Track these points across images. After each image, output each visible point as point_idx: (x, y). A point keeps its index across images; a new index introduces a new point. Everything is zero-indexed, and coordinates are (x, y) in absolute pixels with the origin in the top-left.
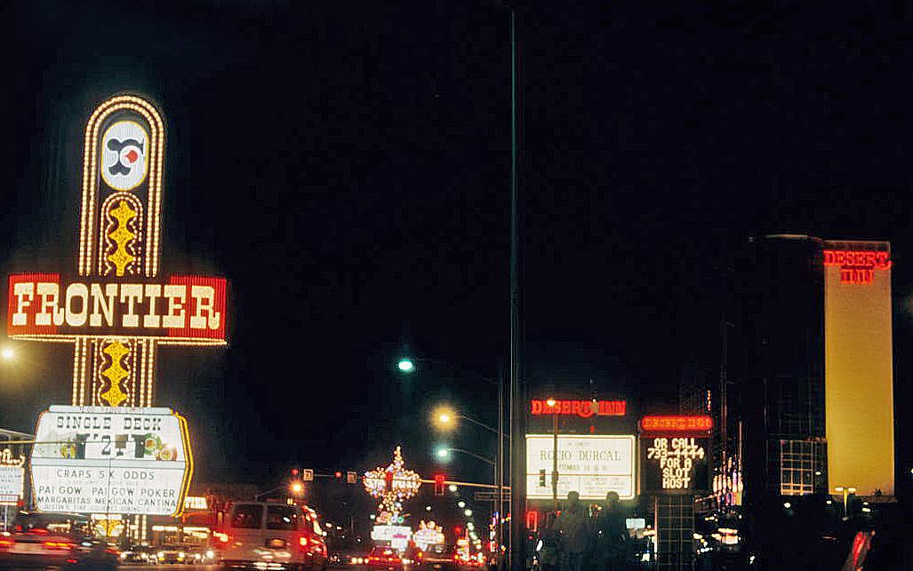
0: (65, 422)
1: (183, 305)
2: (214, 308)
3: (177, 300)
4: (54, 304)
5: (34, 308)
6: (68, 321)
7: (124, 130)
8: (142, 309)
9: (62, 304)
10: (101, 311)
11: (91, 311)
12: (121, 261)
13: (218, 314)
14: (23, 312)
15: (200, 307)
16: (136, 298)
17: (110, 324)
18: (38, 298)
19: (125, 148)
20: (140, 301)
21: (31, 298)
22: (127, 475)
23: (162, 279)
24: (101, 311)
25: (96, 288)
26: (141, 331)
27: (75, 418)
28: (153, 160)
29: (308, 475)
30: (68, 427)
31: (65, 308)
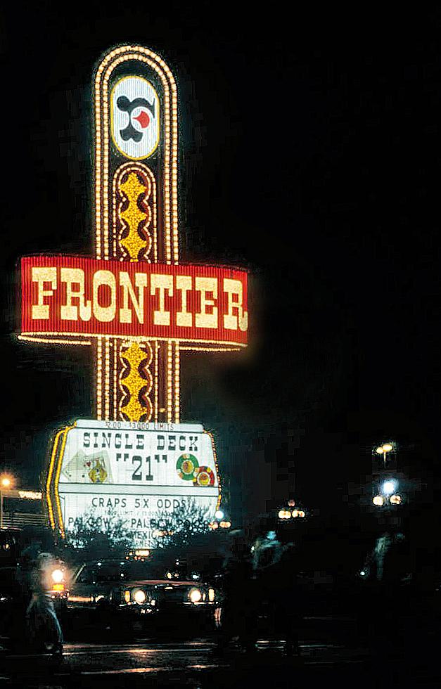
0: (92, 440)
1: (215, 301)
2: (243, 306)
3: (209, 295)
4: (80, 294)
5: (56, 300)
6: (96, 316)
7: (133, 87)
8: (173, 304)
9: (88, 296)
10: (131, 306)
11: (119, 304)
12: (133, 244)
13: (246, 313)
14: (45, 304)
15: (231, 304)
16: (166, 291)
17: (141, 321)
18: (223, 296)
19: (135, 113)
20: (171, 294)
21: (54, 287)
22: (160, 504)
23: (174, 271)
24: (131, 306)
25: (124, 276)
26: (173, 330)
27: (104, 435)
28: (106, 111)
29: (378, 501)
30: (96, 445)
31: (92, 299)
